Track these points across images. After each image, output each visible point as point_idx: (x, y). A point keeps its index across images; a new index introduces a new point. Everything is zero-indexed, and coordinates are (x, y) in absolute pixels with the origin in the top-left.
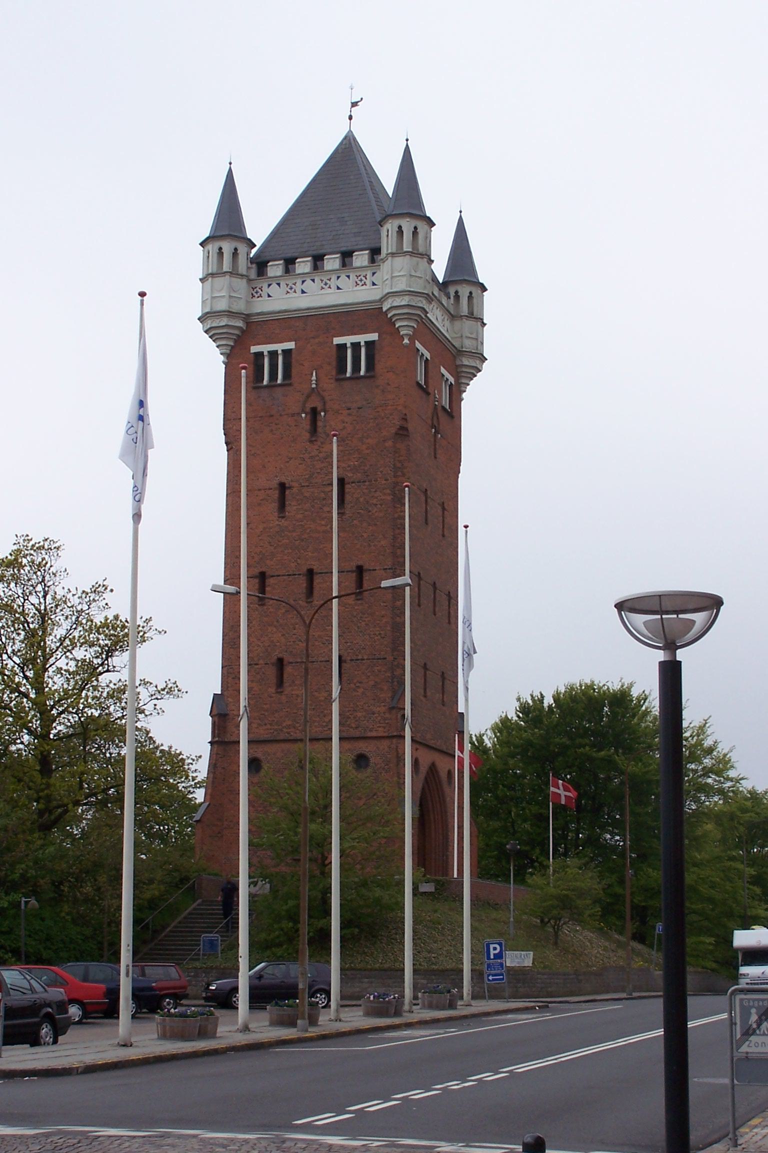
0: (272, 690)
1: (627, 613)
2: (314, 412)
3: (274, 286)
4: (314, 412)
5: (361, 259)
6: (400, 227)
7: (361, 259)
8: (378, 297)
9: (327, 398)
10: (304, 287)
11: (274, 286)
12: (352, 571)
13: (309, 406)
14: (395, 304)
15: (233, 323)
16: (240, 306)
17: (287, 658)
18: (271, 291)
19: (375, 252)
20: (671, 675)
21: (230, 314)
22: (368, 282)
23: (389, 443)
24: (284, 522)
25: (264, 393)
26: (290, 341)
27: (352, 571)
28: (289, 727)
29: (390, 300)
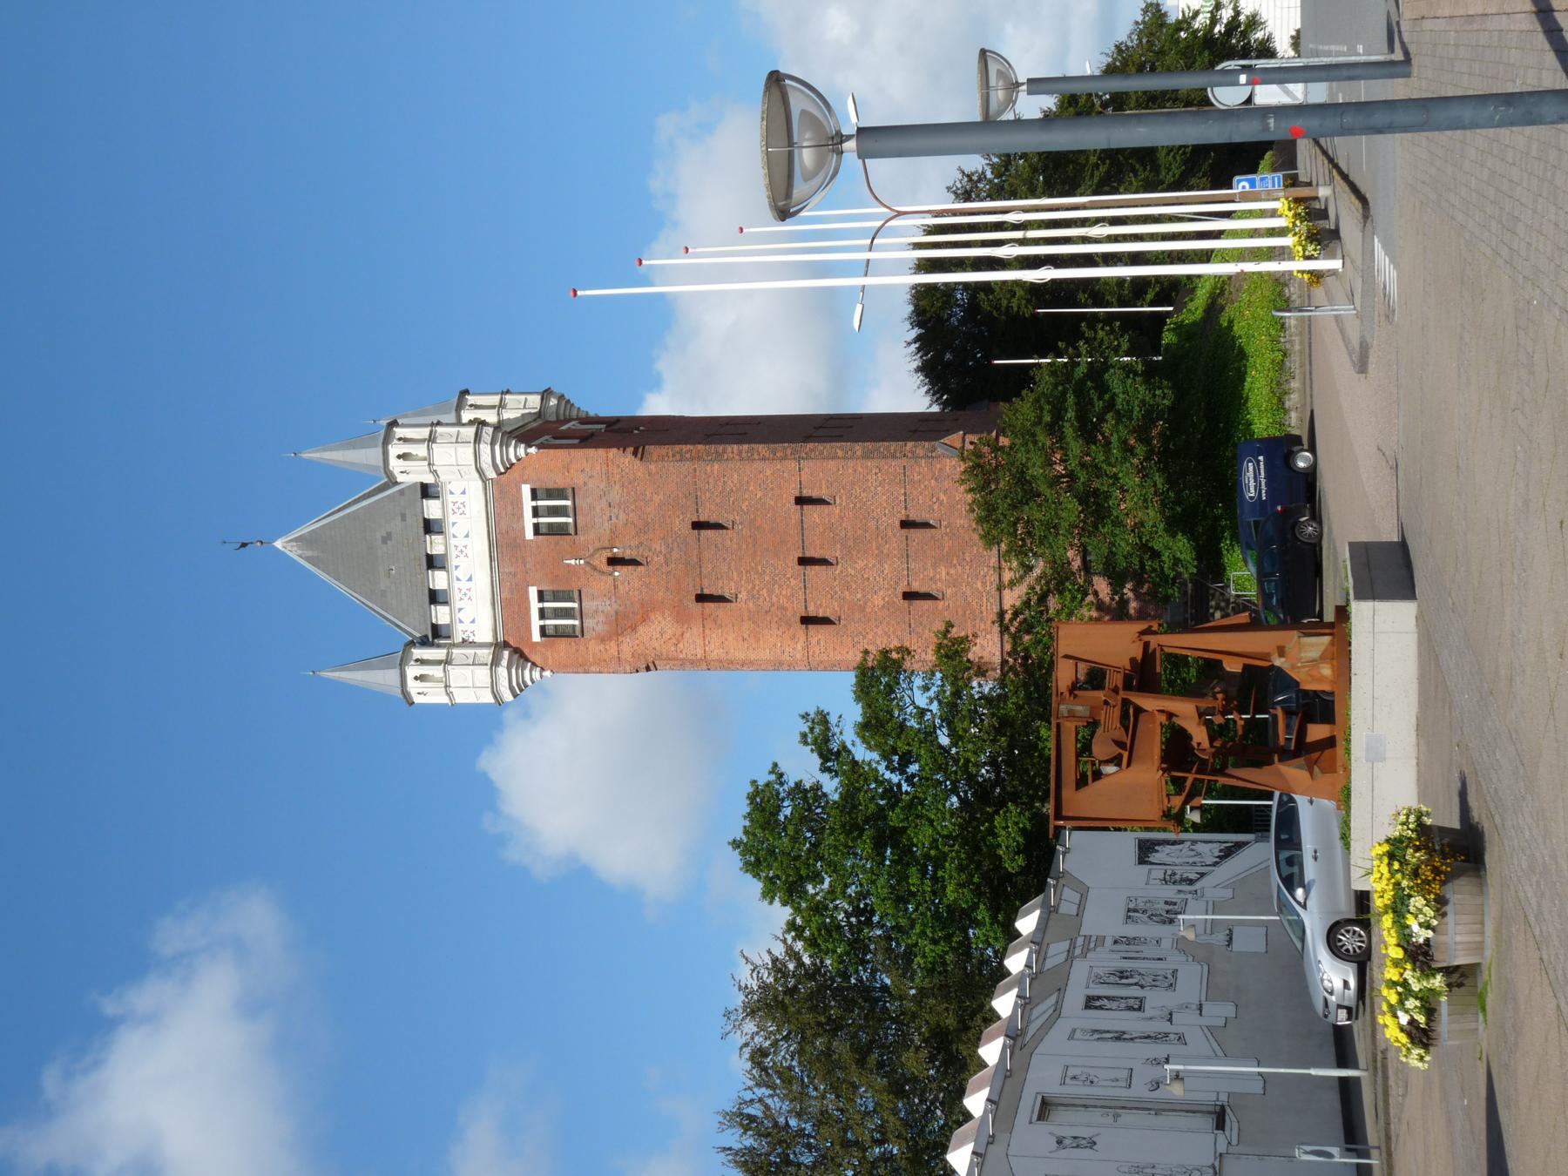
0: (940, 604)
1: (793, 202)
2: (614, 561)
3: (460, 615)
4: (614, 561)
5: (432, 509)
6: (399, 457)
7: (432, 509)
8: (480, 483)
9: (597, 545)
10: (464, 578)
11: (460, 615)
12: (1209, 1113)
13: (605, 567)
14: (489, 460)
15: (505, 662)
16: (486, 654)
17: (902, 587)
18: (467, 621)
19: (426, 491)
20: (880, 140)
21: (495, 662)
22: (461, 499)
23: (652, 467)
24: (743, 596)
25: (588, 623)
26: (527, 593)
27: (1209, 1113)
28: (984, 583)
29: (484, 466)
